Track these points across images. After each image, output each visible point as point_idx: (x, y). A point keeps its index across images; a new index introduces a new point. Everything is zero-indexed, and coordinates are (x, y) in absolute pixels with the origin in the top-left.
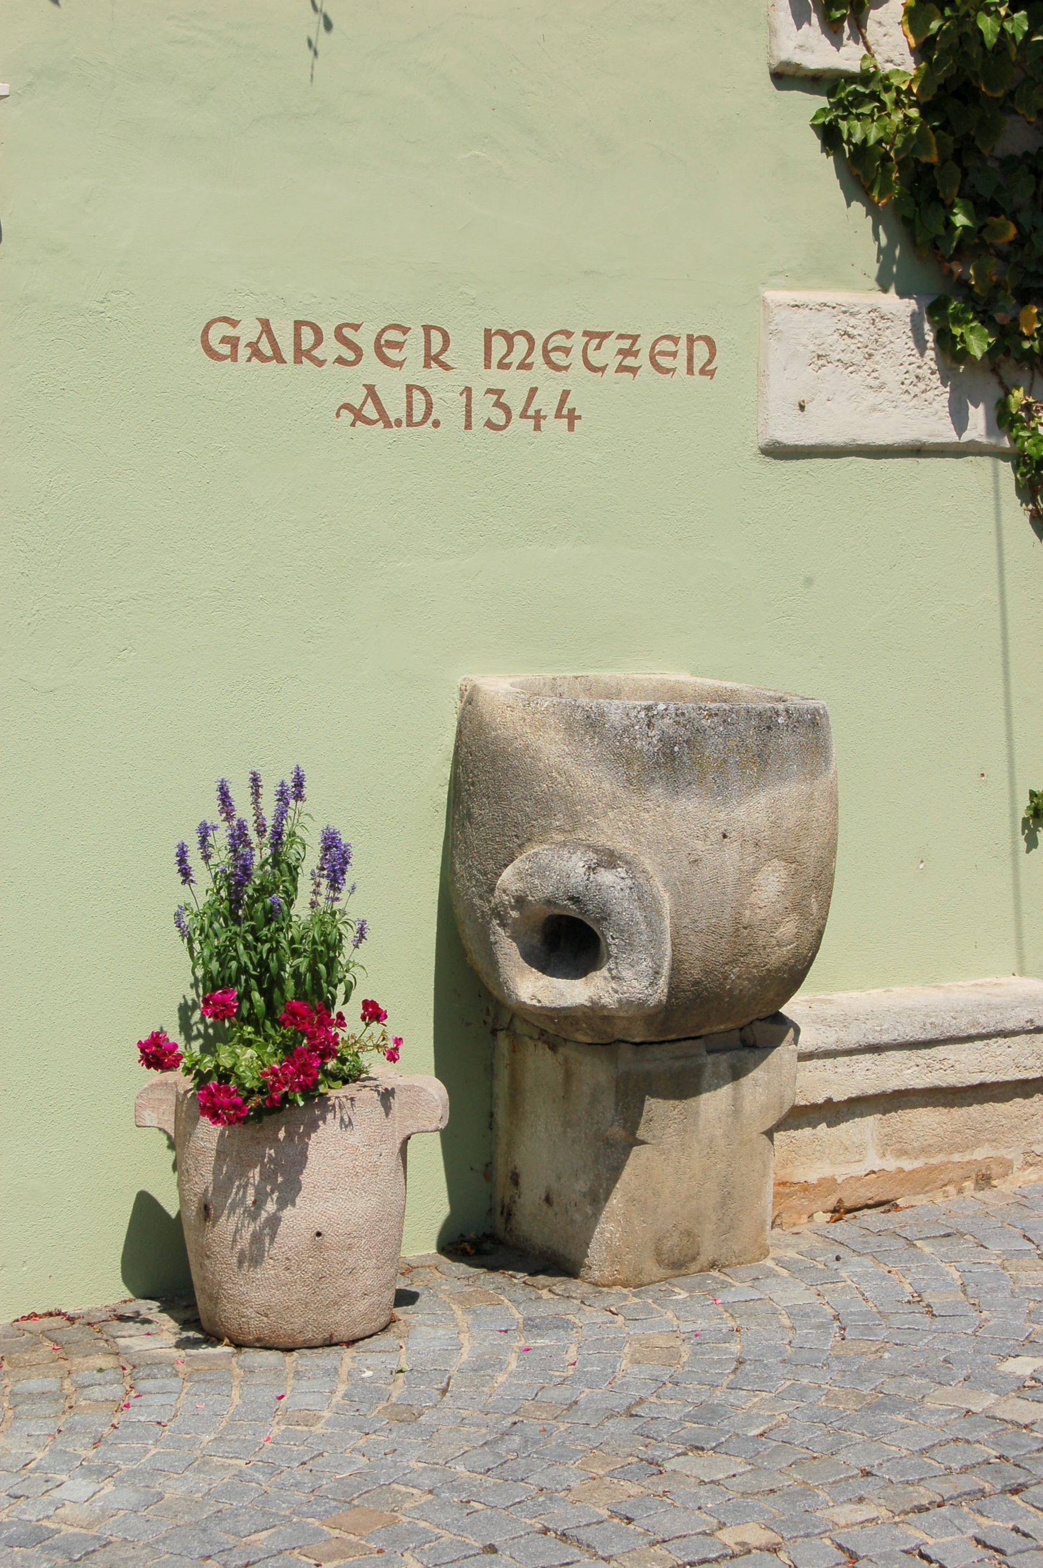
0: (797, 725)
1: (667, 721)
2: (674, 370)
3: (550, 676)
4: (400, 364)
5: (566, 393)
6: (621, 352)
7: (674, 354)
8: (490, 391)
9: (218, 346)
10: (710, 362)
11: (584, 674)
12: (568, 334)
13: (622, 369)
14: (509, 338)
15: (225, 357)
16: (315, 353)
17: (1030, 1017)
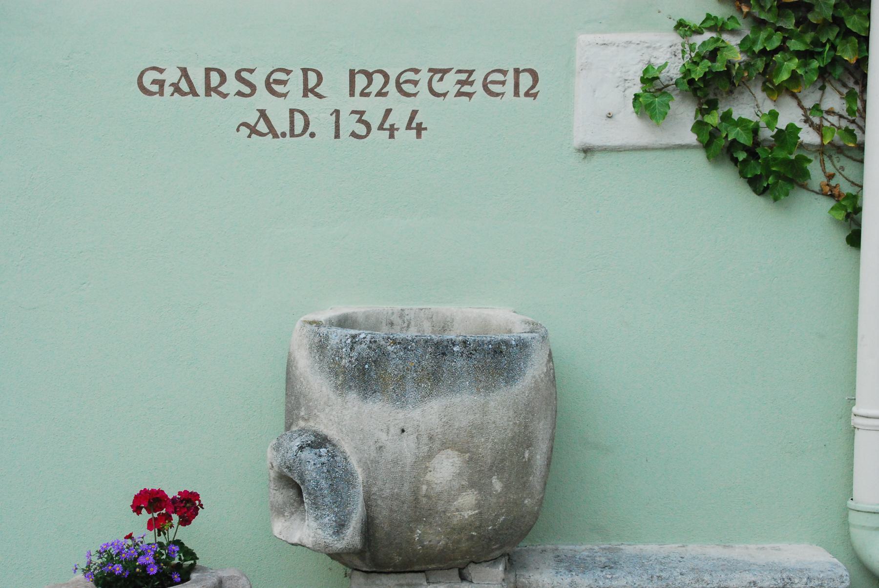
0: (474, 352)
1: (363, 346)
2: (503, 94)
3: (399, 307)
4: (285, 95)
5: (414, 113)
6: (459, 82)
7: (503, 83)
8: (353, 112)
9: (150, 84)
10: (533, 87)
11: (429, 307)
12: (416, 71)
13: (459, 94)
14: (369, 76)
15: (155, 93)
16: (220, 89)
17: (753, 579)
